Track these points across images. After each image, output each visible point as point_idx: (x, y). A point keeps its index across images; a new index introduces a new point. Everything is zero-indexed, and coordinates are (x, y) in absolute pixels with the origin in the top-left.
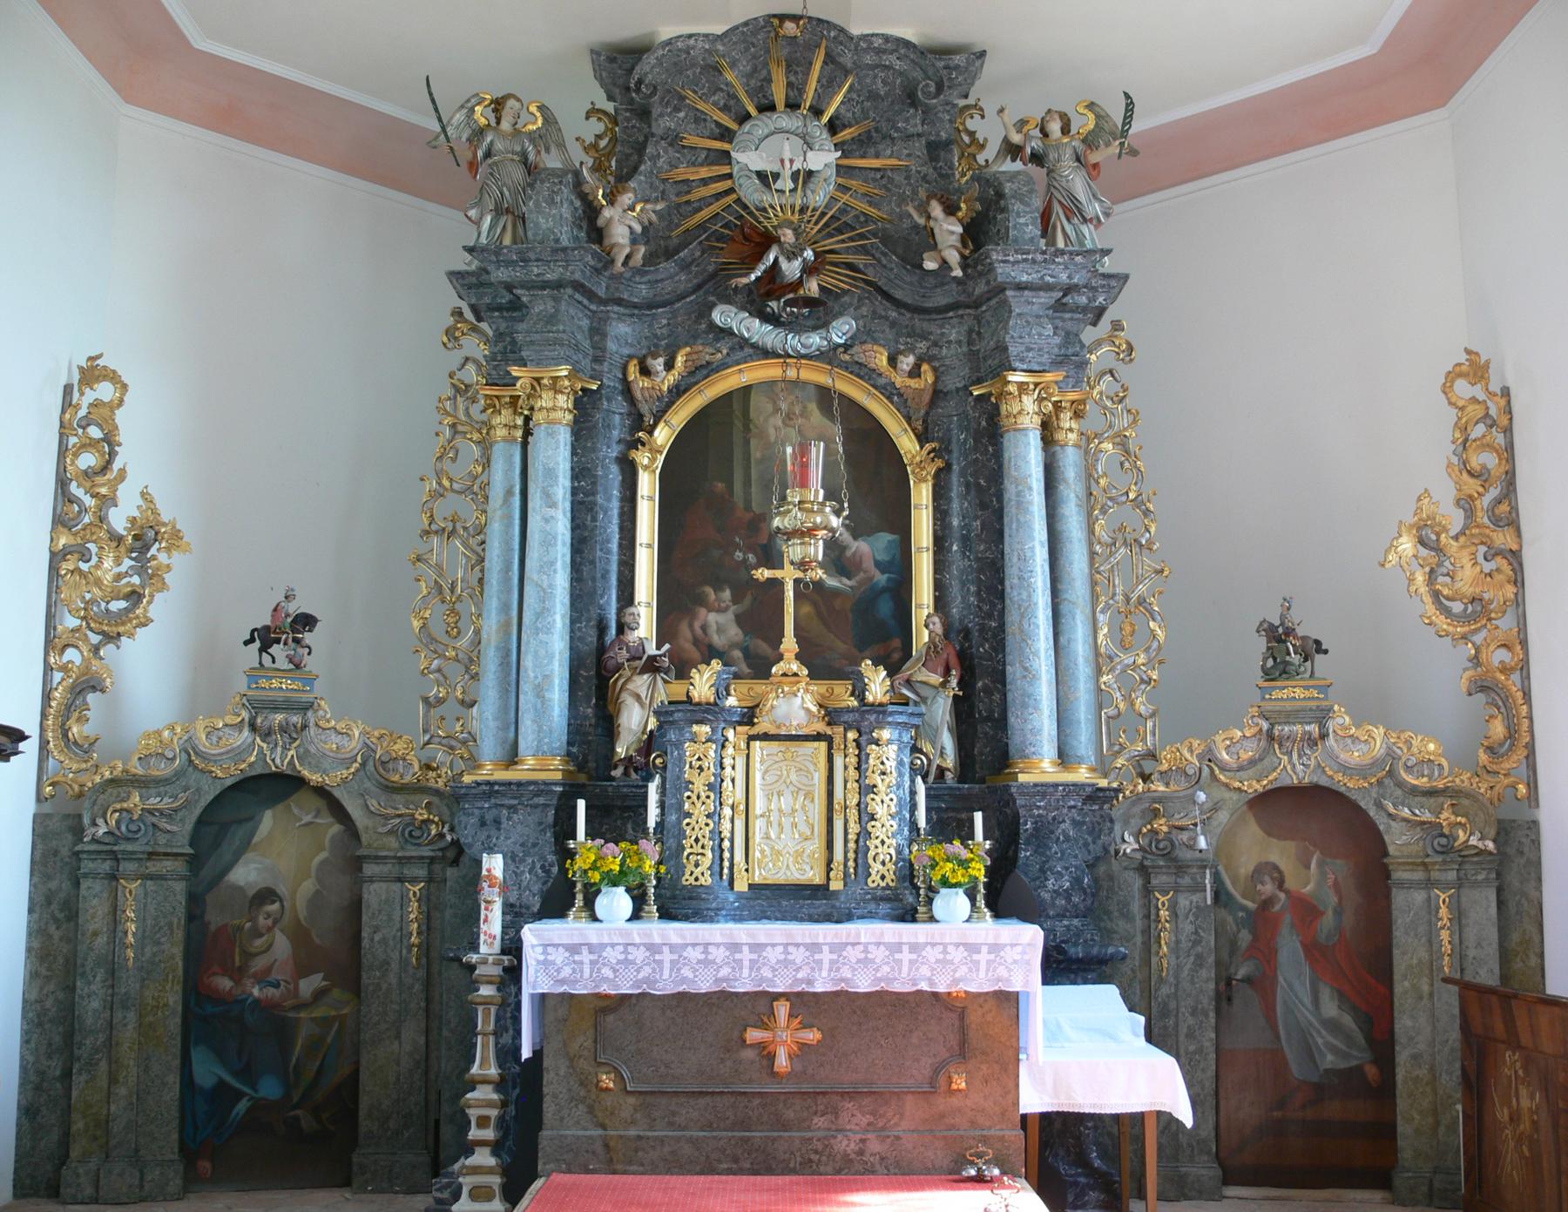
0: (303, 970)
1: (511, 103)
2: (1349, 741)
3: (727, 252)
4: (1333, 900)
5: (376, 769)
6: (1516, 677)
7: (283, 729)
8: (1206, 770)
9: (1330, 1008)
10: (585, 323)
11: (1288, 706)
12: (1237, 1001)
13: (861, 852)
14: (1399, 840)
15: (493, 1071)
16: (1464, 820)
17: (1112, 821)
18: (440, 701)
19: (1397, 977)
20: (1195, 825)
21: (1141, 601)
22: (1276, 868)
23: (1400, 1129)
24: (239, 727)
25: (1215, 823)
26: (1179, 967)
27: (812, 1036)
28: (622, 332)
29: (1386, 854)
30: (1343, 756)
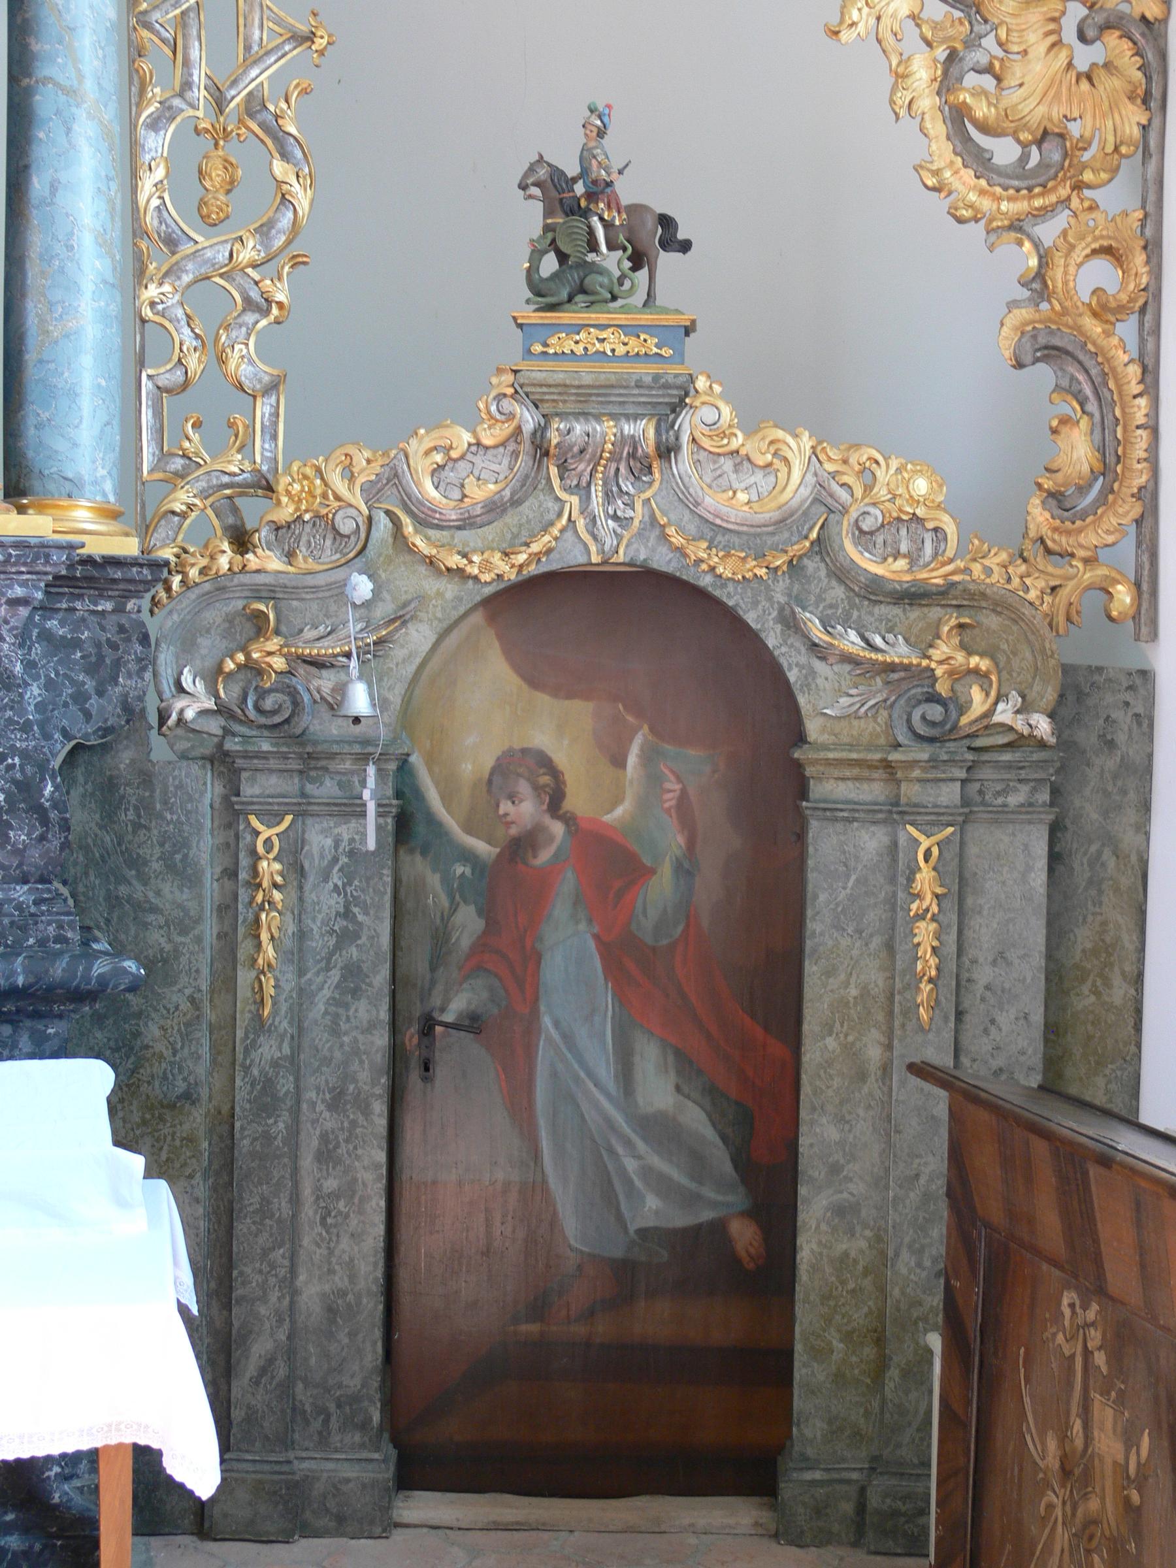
2: (727, 464)
4: (674, 841)
6: (1127, 329)
8: (383, 524)
9: (658, 1090)
11: (587, 374)
12: (441, 1072)
14: (831, 706)
16: (984, 664)
17: (145, 639)
19: (810, 1025)
20: (348, 655)
21: (254, 105)
22: (546, 763)
23: (800, 1373)
25: (398, 653)
26: (304, 995)
29: (800, 738)
30: (712, 502)
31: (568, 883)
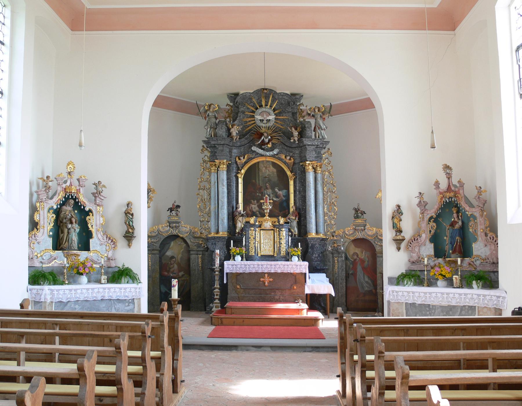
0: (180, 271)
1: (212, 106)
3: (253, 136)
4: (367, 259)
5: (192, 234)
7: (175, 227)
9: (367, 279)
10: (228, 150)
13: (280, 249)
15: (218, 286)
18: (203, 221)
24: (167, 226)
26: (339, 271)
27: (271, 280)
28: (235, 151)
31: (359, 263)
